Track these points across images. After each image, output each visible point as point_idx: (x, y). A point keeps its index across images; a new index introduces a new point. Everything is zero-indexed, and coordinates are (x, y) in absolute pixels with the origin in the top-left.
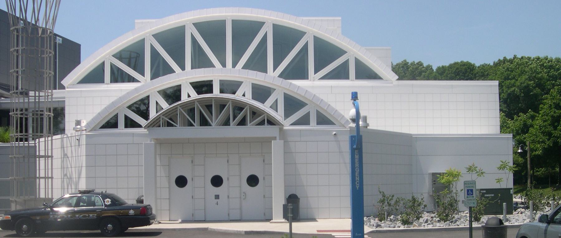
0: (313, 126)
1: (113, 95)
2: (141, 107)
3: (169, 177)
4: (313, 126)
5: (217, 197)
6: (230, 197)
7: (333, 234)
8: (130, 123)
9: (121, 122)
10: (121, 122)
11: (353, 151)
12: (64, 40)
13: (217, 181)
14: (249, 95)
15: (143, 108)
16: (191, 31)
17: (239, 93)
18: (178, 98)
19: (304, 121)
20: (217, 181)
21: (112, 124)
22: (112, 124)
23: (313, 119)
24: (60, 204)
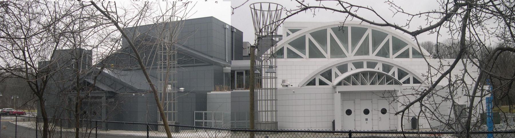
0: (412, 84)
1: (314, 66)
2: (328, 74)
3: (342, 110)
4: (412, 84)
5: (367, 120)
6: (356, 120)
7: (407, 135)
8: (322, 83)
9: (317, 82)
10: (317, 82)
11: (251, 105)
12: (237, 30)
13: (366, 112)
14: (353, 67)
15: (327, 75)
16: (389, 37)
17: (377, 67)
18: (388, 71)
19: (408, 81)
20: (366, 112)
21: (312, 83)
22: (312, 83)
23: (411, 80)
24: (489, 106)
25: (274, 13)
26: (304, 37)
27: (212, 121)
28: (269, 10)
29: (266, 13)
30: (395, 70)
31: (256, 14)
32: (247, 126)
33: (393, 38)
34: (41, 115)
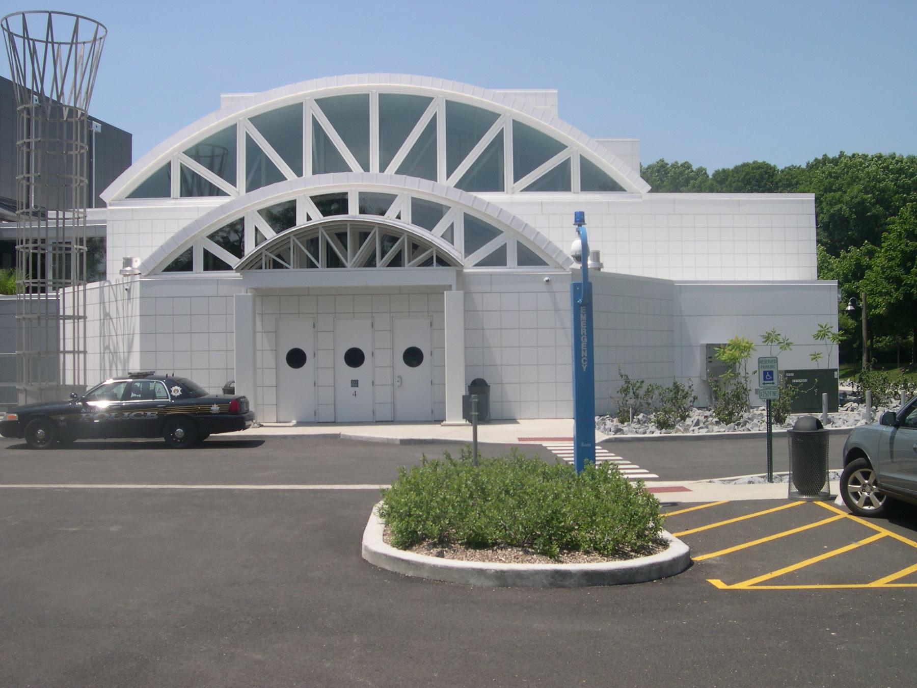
0: (512, 267)
2: (231, 237)
4: (512, 267)
5: (355, 383)
8: (213, 263)
9: (198, 261)
10: (198, 261)
13: (355, 358)
14: (407, 216)
15: (234, 237)
17: (391, 213)
18: (292, 222)
19: (498, 258)
20: (355, 358)
21: (183, 264)
22: (183, 264)
23: (512, 256)
25: (65, 49)
26: (492, 117)
27: (493, 417)
28: (74, 43)
29: (40, 48)
30: (453, 219)
31: (33, 54)
32: (764, 443)
33: (254, 120)
34: (209, 399)
